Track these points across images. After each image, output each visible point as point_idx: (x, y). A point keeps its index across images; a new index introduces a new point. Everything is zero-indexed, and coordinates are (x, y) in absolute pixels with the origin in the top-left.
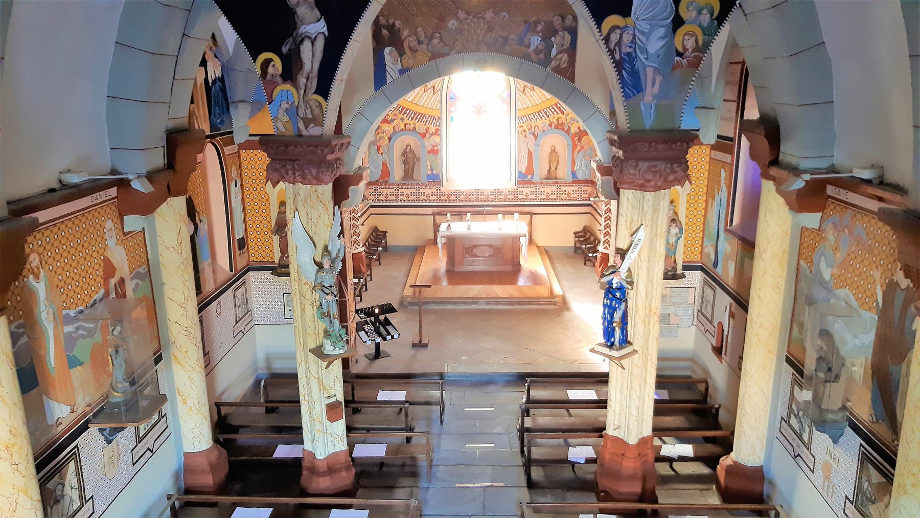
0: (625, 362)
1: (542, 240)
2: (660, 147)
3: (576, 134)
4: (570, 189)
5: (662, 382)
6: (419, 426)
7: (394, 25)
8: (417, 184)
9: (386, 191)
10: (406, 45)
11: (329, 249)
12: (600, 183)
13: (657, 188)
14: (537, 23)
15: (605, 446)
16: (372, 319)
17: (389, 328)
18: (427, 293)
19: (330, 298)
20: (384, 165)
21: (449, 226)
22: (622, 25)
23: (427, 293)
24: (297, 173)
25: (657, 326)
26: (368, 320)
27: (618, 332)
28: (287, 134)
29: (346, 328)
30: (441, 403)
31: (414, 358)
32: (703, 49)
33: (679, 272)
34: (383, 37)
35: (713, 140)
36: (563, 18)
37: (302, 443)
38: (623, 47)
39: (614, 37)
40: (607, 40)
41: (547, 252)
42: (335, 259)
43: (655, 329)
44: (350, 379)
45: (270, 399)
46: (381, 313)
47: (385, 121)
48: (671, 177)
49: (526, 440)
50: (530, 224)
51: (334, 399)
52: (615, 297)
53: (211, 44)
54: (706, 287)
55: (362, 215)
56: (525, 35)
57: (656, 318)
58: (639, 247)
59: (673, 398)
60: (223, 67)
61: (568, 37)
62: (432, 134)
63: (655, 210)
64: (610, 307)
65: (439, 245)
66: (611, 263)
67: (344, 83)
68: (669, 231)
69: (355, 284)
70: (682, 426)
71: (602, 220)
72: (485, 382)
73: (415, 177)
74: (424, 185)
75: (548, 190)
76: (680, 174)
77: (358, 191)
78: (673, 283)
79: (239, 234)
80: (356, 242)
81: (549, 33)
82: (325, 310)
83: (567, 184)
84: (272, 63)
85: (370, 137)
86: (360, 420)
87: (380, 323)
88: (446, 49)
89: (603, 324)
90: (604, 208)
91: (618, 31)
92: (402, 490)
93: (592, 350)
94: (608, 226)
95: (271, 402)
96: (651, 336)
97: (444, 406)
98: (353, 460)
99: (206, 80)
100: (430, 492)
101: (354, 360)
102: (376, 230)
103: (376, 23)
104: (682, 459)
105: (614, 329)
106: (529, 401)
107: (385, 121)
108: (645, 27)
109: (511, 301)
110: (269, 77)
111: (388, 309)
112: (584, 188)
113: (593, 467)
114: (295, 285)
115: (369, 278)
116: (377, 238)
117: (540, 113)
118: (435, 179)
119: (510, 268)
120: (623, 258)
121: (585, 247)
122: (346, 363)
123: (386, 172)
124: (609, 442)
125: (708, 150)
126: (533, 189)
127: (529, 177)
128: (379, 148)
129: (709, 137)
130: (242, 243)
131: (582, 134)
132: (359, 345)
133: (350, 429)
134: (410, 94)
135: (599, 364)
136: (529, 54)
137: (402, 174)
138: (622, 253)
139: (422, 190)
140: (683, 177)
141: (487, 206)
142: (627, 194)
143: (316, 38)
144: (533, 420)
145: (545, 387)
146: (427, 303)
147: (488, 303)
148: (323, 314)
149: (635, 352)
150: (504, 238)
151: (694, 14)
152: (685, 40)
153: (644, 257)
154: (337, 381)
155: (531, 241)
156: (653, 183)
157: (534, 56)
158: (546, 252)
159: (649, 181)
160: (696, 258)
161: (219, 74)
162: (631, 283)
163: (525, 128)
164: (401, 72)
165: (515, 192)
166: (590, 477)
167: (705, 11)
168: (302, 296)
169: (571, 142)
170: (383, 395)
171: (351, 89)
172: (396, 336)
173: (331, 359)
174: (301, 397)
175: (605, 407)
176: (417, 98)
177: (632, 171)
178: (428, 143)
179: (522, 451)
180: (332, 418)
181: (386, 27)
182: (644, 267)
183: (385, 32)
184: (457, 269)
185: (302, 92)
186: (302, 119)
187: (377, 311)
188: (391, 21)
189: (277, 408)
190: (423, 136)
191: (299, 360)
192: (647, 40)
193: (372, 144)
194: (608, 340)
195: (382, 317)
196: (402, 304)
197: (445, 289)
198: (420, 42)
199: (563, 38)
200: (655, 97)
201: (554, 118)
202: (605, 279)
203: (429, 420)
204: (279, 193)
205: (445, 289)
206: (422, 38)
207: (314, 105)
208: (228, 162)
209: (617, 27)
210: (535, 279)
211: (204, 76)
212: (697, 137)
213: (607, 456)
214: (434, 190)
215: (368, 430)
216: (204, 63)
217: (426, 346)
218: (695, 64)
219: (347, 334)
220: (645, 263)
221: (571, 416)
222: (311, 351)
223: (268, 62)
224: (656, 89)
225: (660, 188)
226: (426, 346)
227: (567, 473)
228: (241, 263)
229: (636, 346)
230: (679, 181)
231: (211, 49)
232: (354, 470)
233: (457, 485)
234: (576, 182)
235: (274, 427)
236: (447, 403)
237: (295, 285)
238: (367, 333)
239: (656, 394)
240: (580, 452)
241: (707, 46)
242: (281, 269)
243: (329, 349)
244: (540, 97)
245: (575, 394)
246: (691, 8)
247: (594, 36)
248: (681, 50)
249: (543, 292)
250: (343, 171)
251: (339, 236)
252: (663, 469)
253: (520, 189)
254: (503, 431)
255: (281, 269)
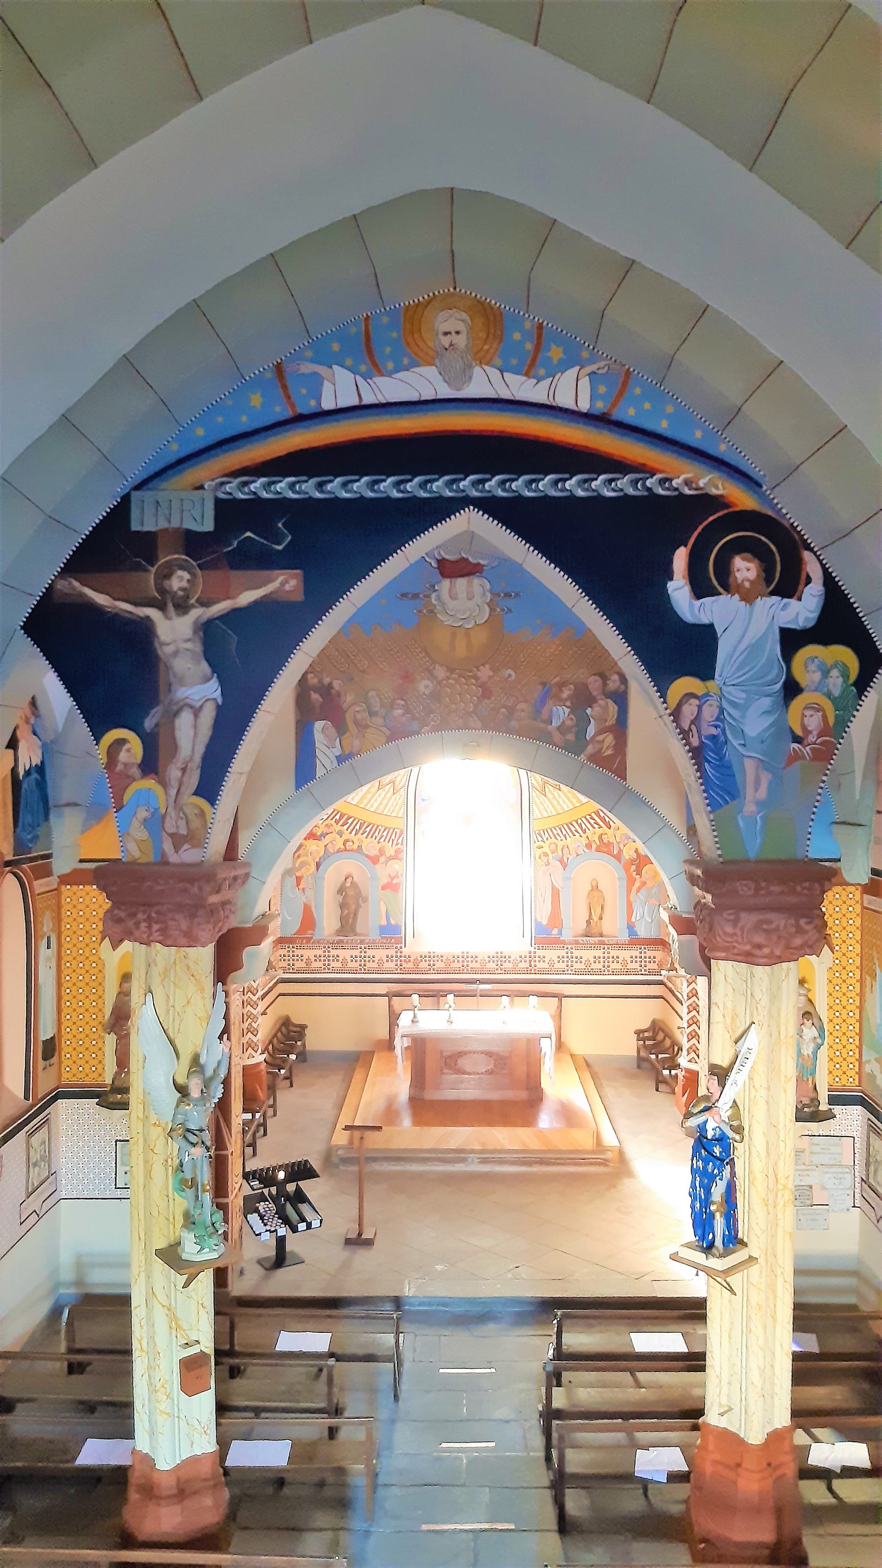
0: (735, 1280)
1: (581, 1042)
2: (775, 888)
3: (632, 862)
4: (625, 954)
5: (805, 1317)
6: (354, 1404)
7: (330, 686)
8: (362, 942)
9: (309, 953)
10: (349, 717)
11: (202, 1060)
12: (675, 946)
13: (774, 960)
14: (562, 685)
15: (703, 1447)
16: (274, 1190)
17: (304, 1208)
18: (374, 1140)
19: (198, 1152)
20: (307, 909)
21: (415, 1016)
22: (700, 693)
23: (374, 1140)
24: (156, 927)
25: (790, 1210)
26: (266, 1191)
27: (719, 1223)
28: (144, 860)
29: (222, 1207)
30: (396, 1358)
31: (346, 1265)
32: (838, 728)
33: (824, 1107)
34: (316, 704)
35: (864, 878)
36: (604, 677)
37: (129, 1434)
38: (704, 726)
39: (689, 710)
40: (676, 714)
41: (588, 1065)
42: (211, 1079)
43: (787, 1215)
44: (229, 1307)
45: (78, 1346)
46: (289, 1179)
47: (312, 836)
48: (798, 941)
49: (555, 1435)
50: (558, 1017)
51: (195, 1350)
52: (712, 1154)
53: (28, 712)
54: (871, 1134)
55: (263, 997)
56: (543, 702)
57: (788, 1195)
58: (750, 1063)
59: (825, 1350)
60: (46, 749)
61: (613, 708)
62: (391, 858)
63: (774, 997)
64: (704, 1173)
65: (398, 1051)
66: (702, 1091)
67: (244, 779)
68: (800, 1034)
69: (246, 1123)
70: (844, 1405)
71: (683, 1010)
72: (474, 1315)
73: (358, 931)
74: (372, 945)
75: (588, 955)
76: (812, 935)
77: (257, 958)
78: (813, 1127)
79: (46, 1032)
80: (250, 1045)
81: (582, 700)
82: (188, 1175)
83: (620, 946)
84: (127, 746)
85: (284, 862)
86: (243, 1391)
87: (288, 1198)
88: (415, 725)
89: (693, 1207)
90: (685, 990)
91: (694, 702)
92: (315, 1534)
93: (674, 1257)
94: (694, 1022)
95: (80, 1351)
96: (780, 1231)
97: (400, 1364)
98: (226, 1472)
99: (14, 771)
100: (372, 1542)
101: (237, 1269)
102: (286, 1022)
103: (303, 682)
104: (849, 1472)
105: (712, 1216)
106: (559, 1354)
107: (312, 836)
108: (738, 695)
109: (526, 1158)
110: (119, 767)
111: (302, 1171)
112: (649, 953)
113: (683, 1490)
114: (137, 1126)
115: (270, 1112)
116: (289, 1037)
117: (570, 827)
118: (392, 934)
119: (523, 1095)
120: (722, 1084)
121: (656, 1057)
122: (221, 1277)
123: (308, 921)
124: (711, 1437)
125: (858, 894)
126: (563, 953)
127: (555, 931)
128: (299, 880)
129: (857, 871)
130: (50, 1048)
131: (641, 862)
132: (248, 1239)
133: (222, 1409)
134: (353, 794)
135: (689, 1284)
136: (550, 733)
137: (336, 925)
138: (721, 1074)
139: (370, 953)
140: (817, 941)
141: (482, 982)
142: (722, 969)
143: (201, 707)
144: (569, 1394)
145: (591, 1326)
146: (375, 1160)
147: (484, 1161)
148: (183, 1182)
149: (751, 1258)
150: (513, 1041)
151: (817, 676)
152: (805, 715)
153: (760, 1080)
154: (202, 1312)
155: (560, 1046)
156: (766, 951)
157: (557, 737)
158: (587, 1066)
159: (759, 947)
160: (850, 1082)
161: (36, 761)
162: (739, 1130)
163: (546, 849)
164: (340, 759)
165: (531, 957)
166: (676, 1509)
167: (835, 673)
168: (149, 1149)
169: (623, 874)
170: (289, 1341)
171: (250, 793)
172: (315, 1224)
173: (192, 1270)
174: (135, 1345)
175: (702, 1369)
176: (368, 799)
177: (729, 929)
178: (383, 872)
179: (548, 1458)
180: (190, 1387)
181: (317, 690)
182: (760, 1099)
183: (315, 697)
184: (431, 1095)
185: (173, 792)
186: (171, 835)
187: (281, 1175)
188: (327, 680)
189: (89, 1364)
190: (374, 860)
191: (135, 1269)
192: (743, 717)
193: (288, 873)
194: (703, 1238)
195: (291, 1187)
196: (328, 1157)
197: (407, 1134)
198: (372, 714)
199: (605, 708)
200: (760, 804)
201: (593, 834)
202: (693, 1122)
203: (372, 1390)
204: (123, 957)
205: (407, 1134)
206: (376, 707)
207: (190, 812)
208: (39, 906)
209: (692, 695)
210: (568, 1115)
211: (12, 765)
212: (835, 873)
213: (709, 1469)
214: (392, 952)
215: (257, 1411)
216: (13, 744)
217: (369, 1243)
218: (825, 754)
219: (226, 1220)
220: (763, 1093)
221: (638, 1385)
222: (159, 1253)
223: (120, 742)
224: (762, 793)
225: (780, 960)
226: (369, 1243)
227: (630, 1503)
228: (45, 1084)
229: (753, 1250)
230: (810, 947)
231: (27, 721)
232: (226, 1494)
233: (425, 1527)
234: (635, 941)
235: (82, 1403)
236: (407, 1356)
237: (137, 1126)
238: (262, 1217)
239: (795, 1341)
240: (658, 1461)
241: (842, 724)
242: (113, 1097)
243: (190, 1250)
244: (567, 801)
245: (645, 1342)
246: (812, 667)
247: (656, 707)
248: (799, 732)
249: (582, 1140)
250: (234, 922)
251: (220, 1038)
252: (814, 1493)
253: (540, 953)
254: (512, 1416)
255: (113, 1097)
